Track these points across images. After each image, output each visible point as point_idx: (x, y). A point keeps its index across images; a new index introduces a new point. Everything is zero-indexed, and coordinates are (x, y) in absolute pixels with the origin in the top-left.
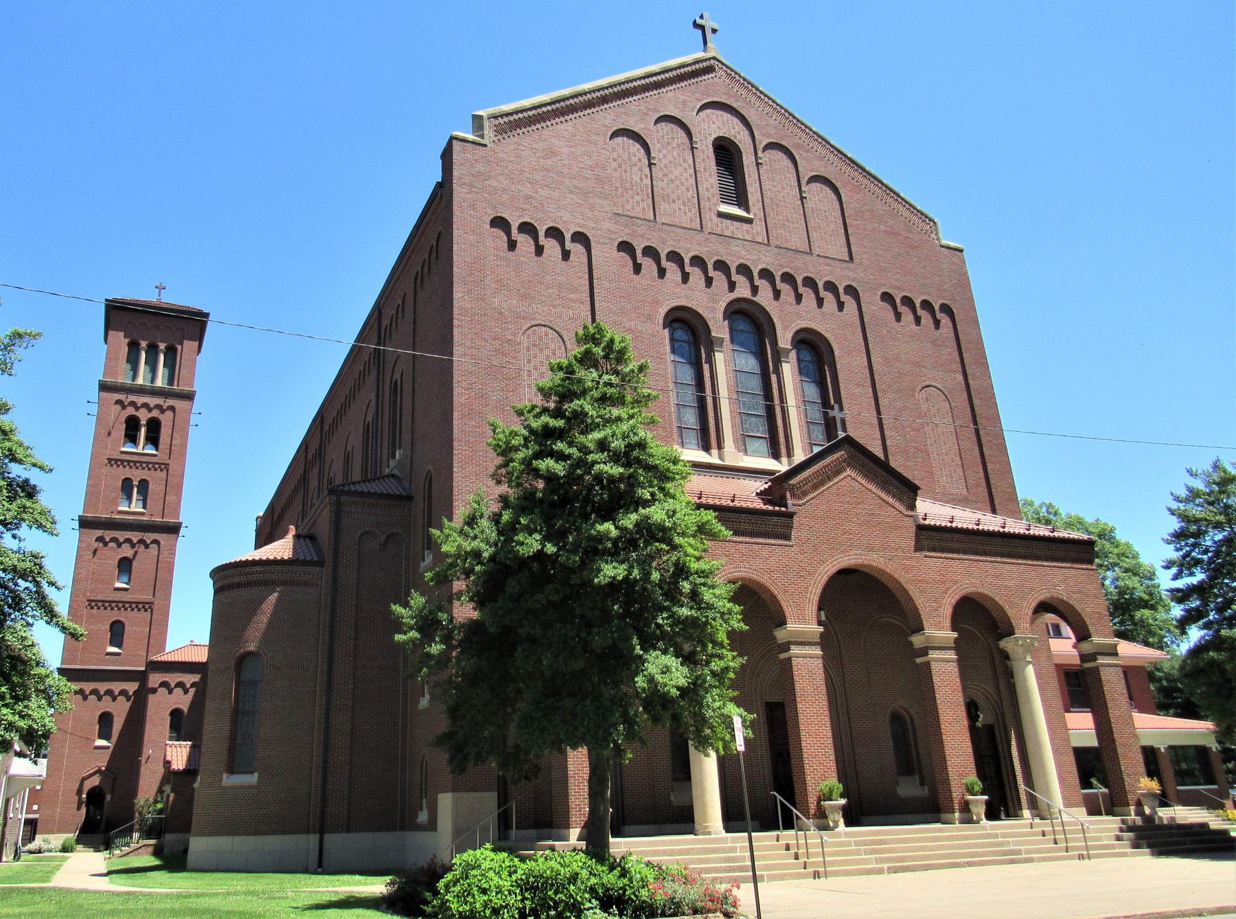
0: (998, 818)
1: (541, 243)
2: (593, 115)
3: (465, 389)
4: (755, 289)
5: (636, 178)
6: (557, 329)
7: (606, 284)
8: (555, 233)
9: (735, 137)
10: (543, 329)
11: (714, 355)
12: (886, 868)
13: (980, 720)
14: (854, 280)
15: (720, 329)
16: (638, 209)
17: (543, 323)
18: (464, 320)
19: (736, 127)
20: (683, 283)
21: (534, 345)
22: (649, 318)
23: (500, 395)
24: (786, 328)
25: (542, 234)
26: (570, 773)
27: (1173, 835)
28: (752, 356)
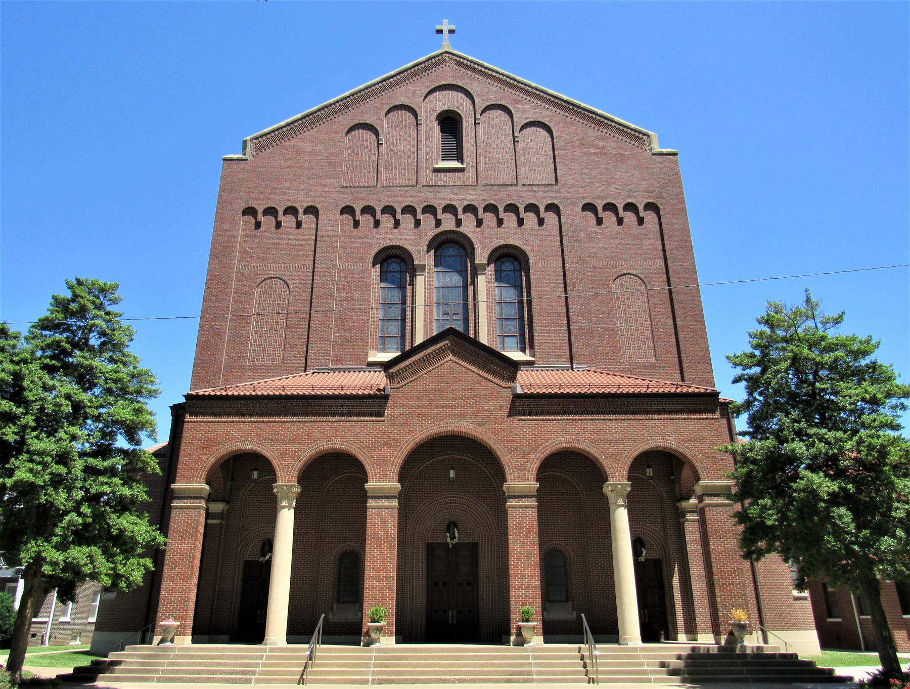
0: (657, 640)
1: (279, 219)
2: (334, 120)
3: (207, 331)
4: (459, 223)
5: (366, 157)
6: (285, 279)
7: (326, 239)
8: (630, 207)
9: (458, 108)
10: (274, 280)
11: (477, 278)
12: (370, 680)
13: (643, 555)
14: (556, 198)
15: (424, 258)
16: (363, 180)
17: (273, 276)
18: (213, 283)
19: (460, 100)
20: (394, 228)
21: (265, 293)
22: (362, 259)
23: (234, 332)
24: (483, 248)
25: (542, 209)
26: (162, 597)
27: (539, 673)
28: (457, 274)
